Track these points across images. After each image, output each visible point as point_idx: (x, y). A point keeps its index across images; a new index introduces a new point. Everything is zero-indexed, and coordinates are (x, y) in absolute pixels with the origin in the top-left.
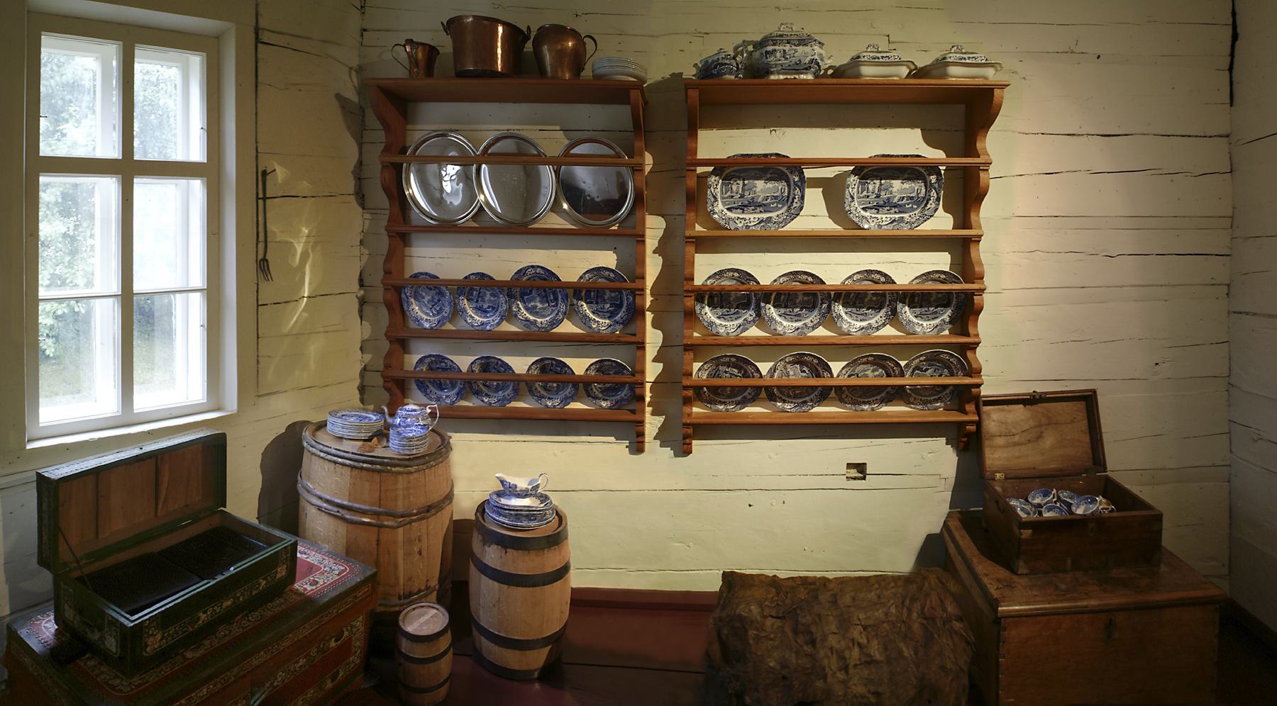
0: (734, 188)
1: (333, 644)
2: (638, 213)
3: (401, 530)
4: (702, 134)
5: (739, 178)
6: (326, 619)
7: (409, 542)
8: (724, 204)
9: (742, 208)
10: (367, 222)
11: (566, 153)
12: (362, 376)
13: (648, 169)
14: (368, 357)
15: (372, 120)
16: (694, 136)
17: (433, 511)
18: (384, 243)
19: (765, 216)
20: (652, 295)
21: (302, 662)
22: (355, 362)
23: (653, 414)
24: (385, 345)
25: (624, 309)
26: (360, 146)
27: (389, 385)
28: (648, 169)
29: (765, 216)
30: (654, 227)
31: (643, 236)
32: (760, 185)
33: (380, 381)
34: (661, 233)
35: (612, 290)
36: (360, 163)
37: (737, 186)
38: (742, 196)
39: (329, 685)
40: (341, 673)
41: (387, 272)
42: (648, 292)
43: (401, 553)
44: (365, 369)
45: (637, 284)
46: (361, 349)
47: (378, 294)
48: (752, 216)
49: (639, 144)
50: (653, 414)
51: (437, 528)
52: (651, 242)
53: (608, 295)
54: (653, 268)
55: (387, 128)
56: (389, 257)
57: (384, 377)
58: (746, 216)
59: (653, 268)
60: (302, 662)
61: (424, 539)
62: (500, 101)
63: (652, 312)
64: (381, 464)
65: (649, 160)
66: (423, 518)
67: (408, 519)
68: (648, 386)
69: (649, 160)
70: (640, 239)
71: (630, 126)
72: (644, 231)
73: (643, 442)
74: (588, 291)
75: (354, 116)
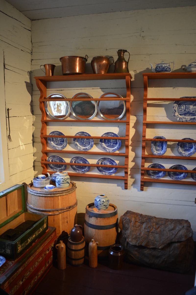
0: (182, 108)
1: (47, 252)
2: (127, 115)
3: (60, 215)
4: (149, 89)
5: (184, 104)
6: (46, 244)
7: (63, 218)
8: (178, 113)
9: (185, 114)
10: (34, 119)
11: (102, 97)
12: (34, 163)
13: (131, 100)
14: (36, 158)
15: (35, 87)
16: (146, 89)
17: (71, 208)
18: (40, 125)
19: (193, 117)
20: (132, 141)
21: (41, 258)
22: (31, 159)
23: (131, 178)
24: (41, 155)
25: (118, 144)
26: (32, 96)
27: (43, 165)
28: (131, 100)
29: (193, 117)
30: (133, 119)
31: (129, 122)
32: (191, 107)
33: (40, 164)
34: (135, 121)
35: (113, 139)
36: (32, 101)
37: (183, 107)
38: (185, 110)
39: (47, 265)
40: (50, 261)
41: (42, 134)
42: (130, 140)
43: (61, 222)
44: (35, 161)
45: (127, 138)
46: (33, 155)
47: (39, 139)
48: (188, 117)
49: (128, 93)
50: (131, 178)
51: (72, 215)
52: (132, 124)
53: (112, 141)
54: (132, 132)
55: (41, 90)
56: (42, 129)
57: (41, 163)
58: (186, 117)
59: (132, 132)
60: (41, 258)
61: (69, 217)
62: (111, 79)
63: (132, 146)
64: (53, 194)
65: (132, 98)
66: (67, 211)
67: (63, 211)
68: (129, 169)
69: (132, 98)
70: (128, 124)
71: (125, 86)
72: (129, 121)
73: (127, 186)
74: (105, 140)
75: (30, 87)
